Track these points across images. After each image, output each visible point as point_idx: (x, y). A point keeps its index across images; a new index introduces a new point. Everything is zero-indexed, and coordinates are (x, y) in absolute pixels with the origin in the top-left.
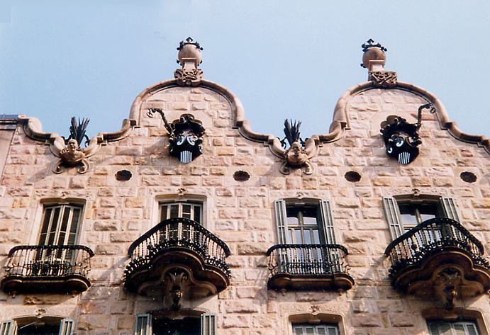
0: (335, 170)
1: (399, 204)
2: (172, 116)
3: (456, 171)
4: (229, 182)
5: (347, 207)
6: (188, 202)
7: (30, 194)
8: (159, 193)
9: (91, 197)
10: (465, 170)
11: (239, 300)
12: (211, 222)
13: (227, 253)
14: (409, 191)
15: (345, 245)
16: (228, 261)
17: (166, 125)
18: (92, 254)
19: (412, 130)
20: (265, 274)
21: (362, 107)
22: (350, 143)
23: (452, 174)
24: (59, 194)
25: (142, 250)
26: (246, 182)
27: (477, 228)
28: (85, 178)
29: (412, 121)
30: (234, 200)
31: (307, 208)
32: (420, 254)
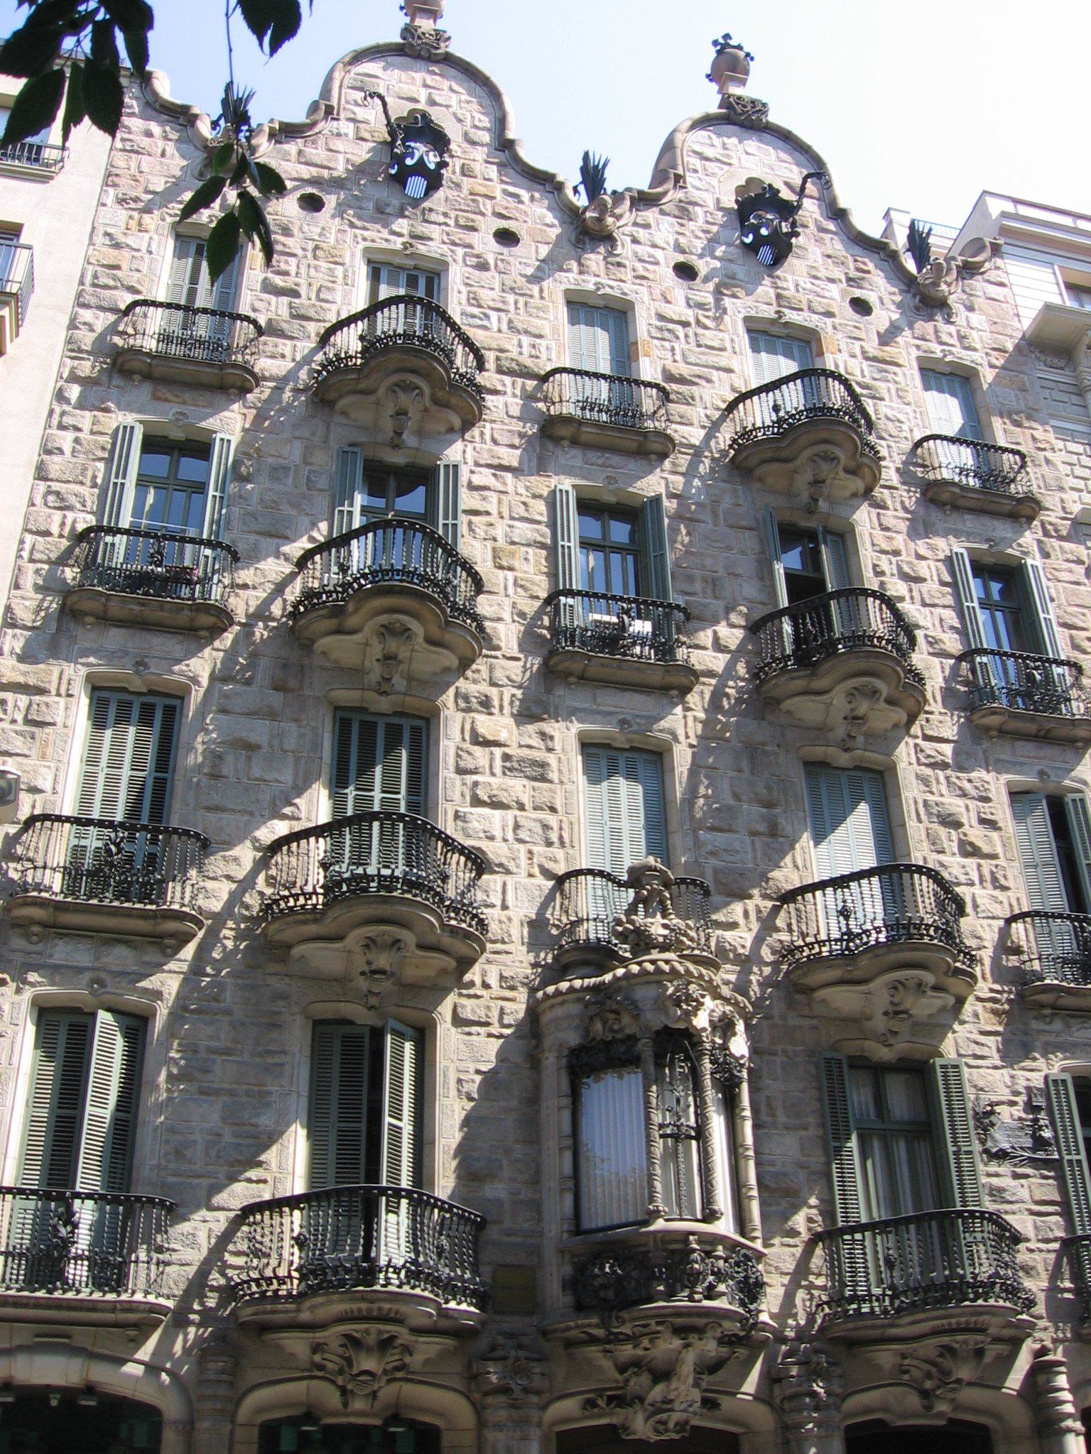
32: (350, 584)
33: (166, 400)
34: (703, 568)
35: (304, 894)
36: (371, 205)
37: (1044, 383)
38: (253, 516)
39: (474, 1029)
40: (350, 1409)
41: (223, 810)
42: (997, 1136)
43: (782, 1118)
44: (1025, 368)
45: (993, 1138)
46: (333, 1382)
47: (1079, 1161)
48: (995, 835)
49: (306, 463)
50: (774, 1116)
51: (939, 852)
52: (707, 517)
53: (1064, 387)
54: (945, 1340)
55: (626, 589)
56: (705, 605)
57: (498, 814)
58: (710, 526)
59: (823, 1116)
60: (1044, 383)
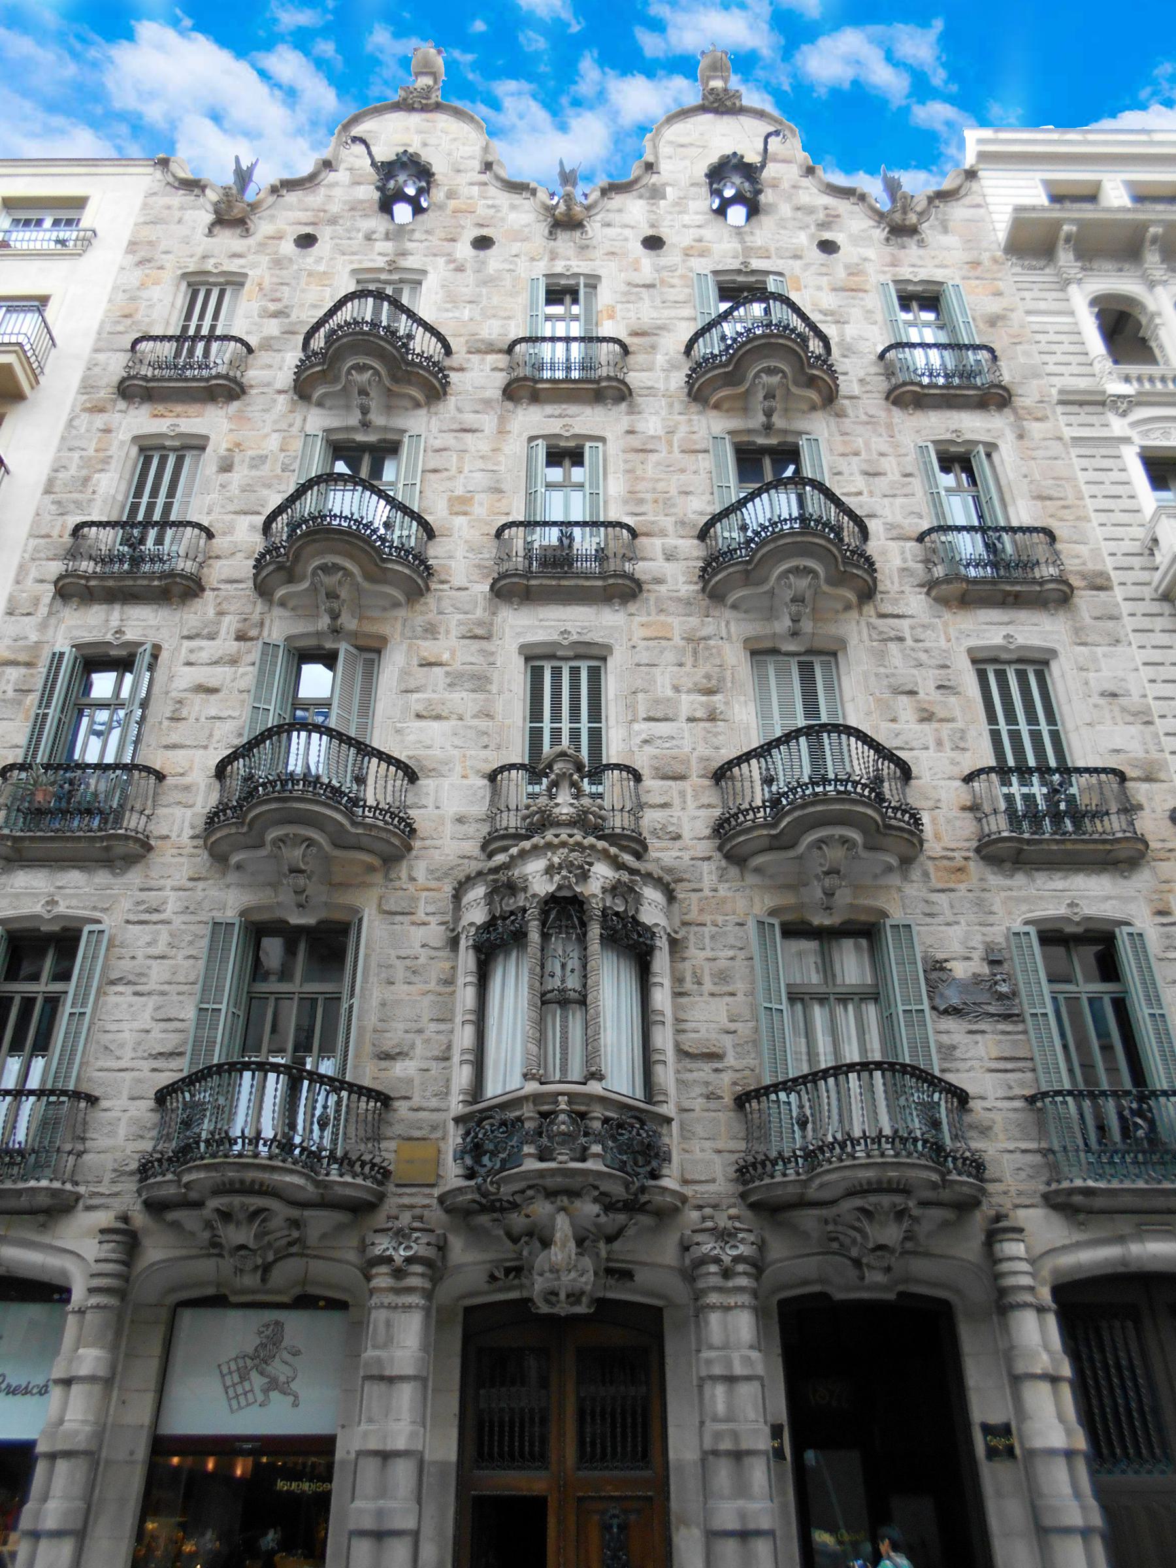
0: (627, 232)
1: (938, 453)
2: (384, 152)
3: (812, 236)
4: (463, 249)
5: (637, 286)
6: (401, 281)
7: (168, 265)
8: (356, 266)
9: (258, 271)
10: (827, 236)
11: (459, 416)
12: (427, 303)
13: (448, 351)
14: (735, 264)
15: (627, 340)
16: (447, 362)
17: (373, 164)
18: (250, 350)
19: (750, 172)
20: (501, 379)
21: (683, 140)
22: (656, 193)
23: (804, 240)
24: (209, 266)
25: (318, 342)
26: (489, 252)
27: (829, 318)
28: (251, 241)
29: (752, 158)
30: (469, 277)
31: (925, 298)
32: (752, 540)
33: (162, 416)
34: (654, 490)
35: (752, 809)
36: (360, 235)
37: (1020, 286)
38: (231, 500)
39: (399, 918)
40: (269, 1286)
41: (182, 747)
42: (947, 992)
43: (708, 986)
44: (1000, 275)
45: (942, 995)
46: (292, 1255)
47: (1045, 1015)
48: (953, 699)
49: (282, 450)
50: (699, 983)
51: (893, 720)
52: (663, 447)
53: (1046, 286)
54: (858, 1202)
55: (968, 516)
56: (653, 523)
57: (435, 725)
58: (664, 454)
59: (753, 982)
60: (1020, 286)
